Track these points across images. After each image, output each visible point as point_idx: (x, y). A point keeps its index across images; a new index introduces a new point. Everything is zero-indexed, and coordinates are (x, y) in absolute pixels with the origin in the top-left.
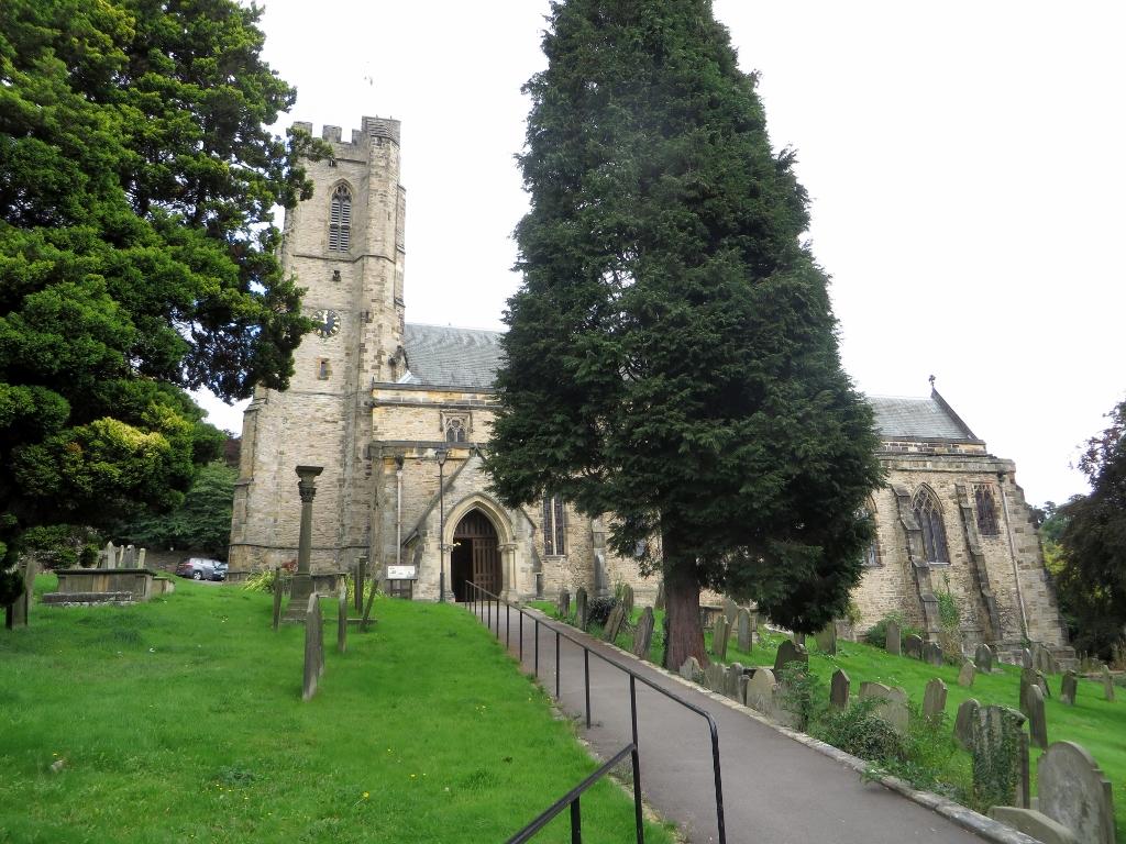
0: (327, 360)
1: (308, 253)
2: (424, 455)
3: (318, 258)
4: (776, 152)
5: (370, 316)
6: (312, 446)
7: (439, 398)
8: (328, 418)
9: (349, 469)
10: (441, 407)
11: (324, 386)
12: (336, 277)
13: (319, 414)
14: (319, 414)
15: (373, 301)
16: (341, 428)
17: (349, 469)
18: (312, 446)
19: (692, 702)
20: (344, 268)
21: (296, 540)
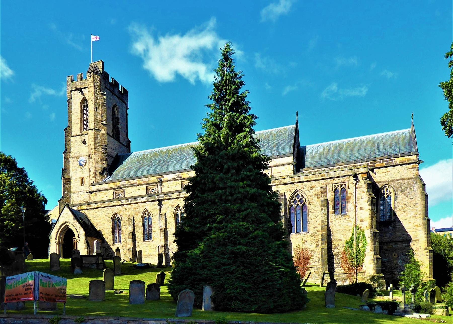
12: (84, 142)
15: (91, 149)
21: (72, 139)
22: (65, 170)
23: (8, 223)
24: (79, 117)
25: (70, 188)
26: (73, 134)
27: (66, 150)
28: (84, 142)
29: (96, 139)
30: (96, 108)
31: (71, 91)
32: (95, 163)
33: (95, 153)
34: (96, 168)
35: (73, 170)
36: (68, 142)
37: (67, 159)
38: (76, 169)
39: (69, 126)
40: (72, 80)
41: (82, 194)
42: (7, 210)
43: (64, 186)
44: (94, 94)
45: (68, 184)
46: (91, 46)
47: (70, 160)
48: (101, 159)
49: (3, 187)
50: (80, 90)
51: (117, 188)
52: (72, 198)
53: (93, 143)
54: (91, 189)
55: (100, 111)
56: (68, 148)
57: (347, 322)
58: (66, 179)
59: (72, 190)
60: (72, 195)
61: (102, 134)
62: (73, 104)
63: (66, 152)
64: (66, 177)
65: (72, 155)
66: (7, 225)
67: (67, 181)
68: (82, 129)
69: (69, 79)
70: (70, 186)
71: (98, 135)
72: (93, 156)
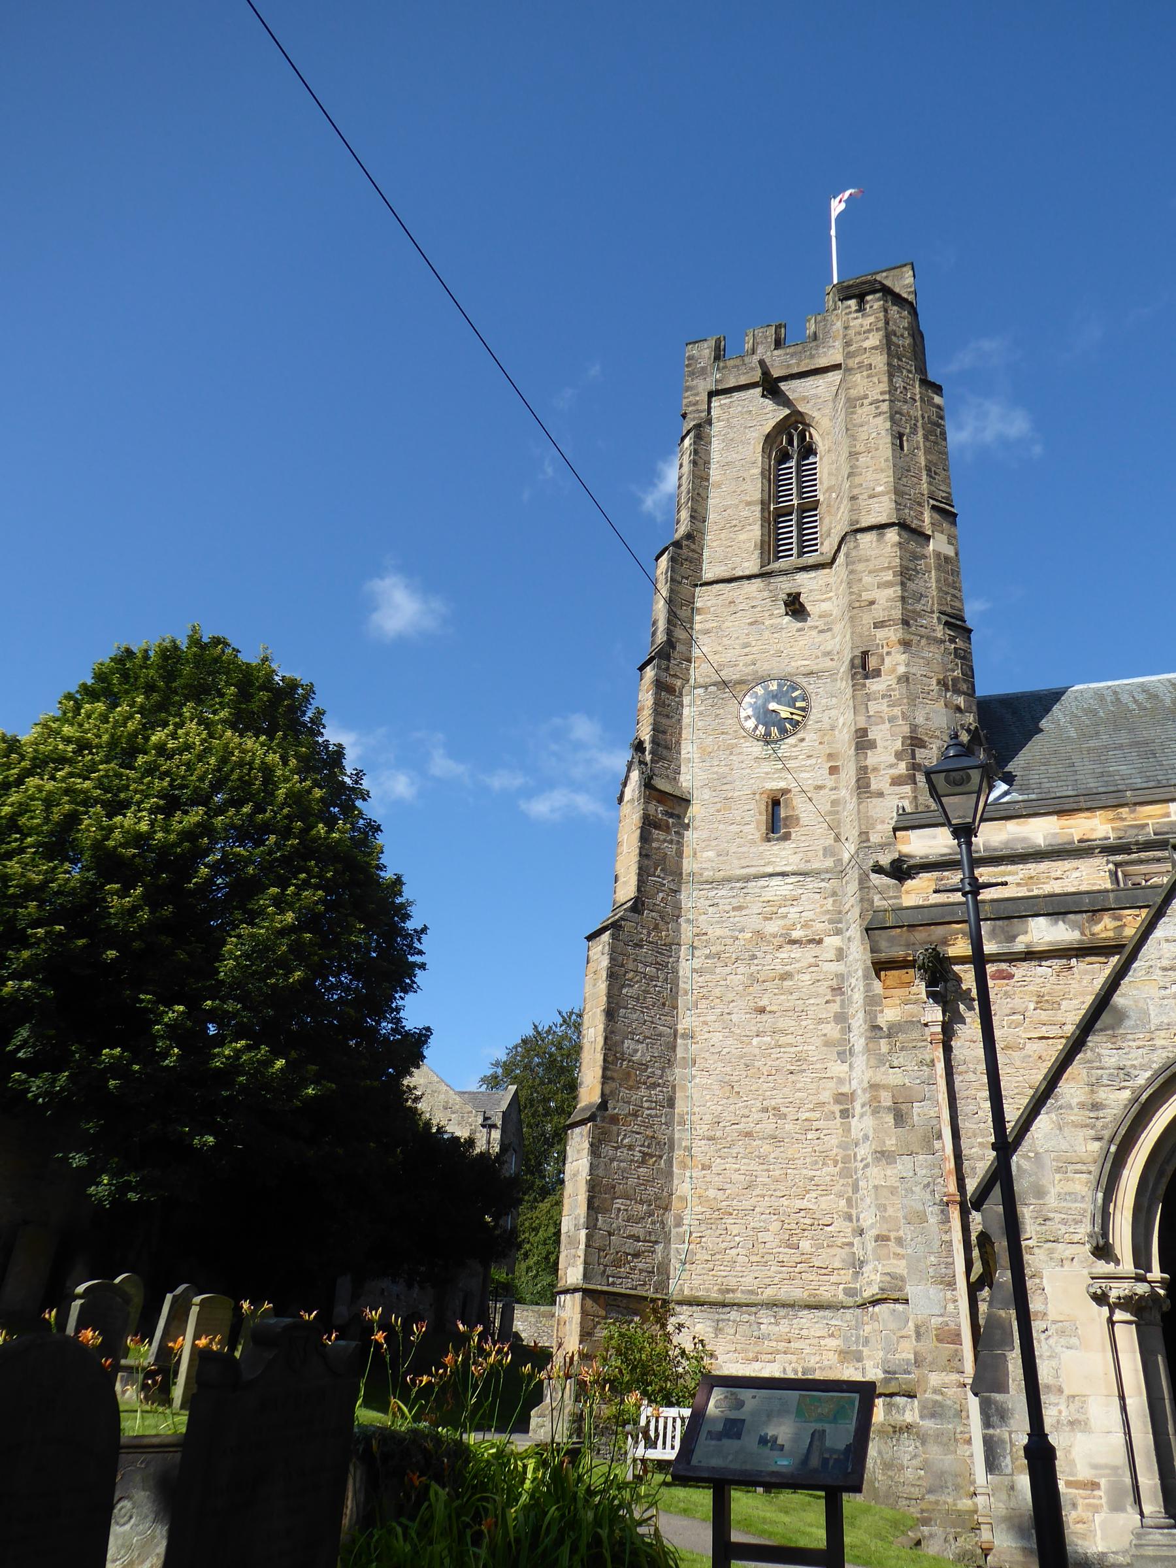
0: (785, 792)
1: (727, 575)
2: (1020, 945)
3: (749, 577)
4: (388, 875)
5: (872, 663)
6: (762, 1011)
7: (1097, 826)
8: (796, 935)
9: (860, 1061)
10: (1108, 850)
11: (783, 855)
12: (795, 607)
13: (772, 927)
14: (772, 927)
15: (878, 625)
16: (831, 955)
17: (860, 1061)
18: (762, 1011)
19: (1003, 814)
20: (807, 584)
21: (704, 598)
22: (658, 754)
23: (238, 1053)
24: (757, 496)
25: (680, 854)
26: (708, 574)
27: (670, 643)
28: (795, 607)
29: (906, 574)
30: (901, 436)
31: (711, 394)
32: (912, 700)
33: (906, 644)
34: (914, 728)
35: (706, 755)
36: (680, 610)
37: (670, 690)
38: (731, 749)
39: (689, 536)
40: (719, 355)
41: (768, 895)
42: (261, 950)
43: (645, 838)
44: (891, 376)
45: (667, 829)
46: (833, 232)
47: (686, 700)
48: (942, 683)
49: (259, 809)
50: (771, 387)
51: (1148, 846)
52: (688, 913)
53: (895, 592)
54: (905, 849)
55: (921, 453)
56: (680, 634)
57: (863, 1565)
58: (663, 797)
59: (688, 865)
60: (689, 898)
61: (938, 555)
62: (716, 445)
63: (669, 656)
64: (661, 784)
65: (699, 672)
66: (234, 1066)
67: (666, 810)
68: (772, 547)
69: (705, 352)
70: (680, 844)
71: (915, 557)
72: (896, 662)
